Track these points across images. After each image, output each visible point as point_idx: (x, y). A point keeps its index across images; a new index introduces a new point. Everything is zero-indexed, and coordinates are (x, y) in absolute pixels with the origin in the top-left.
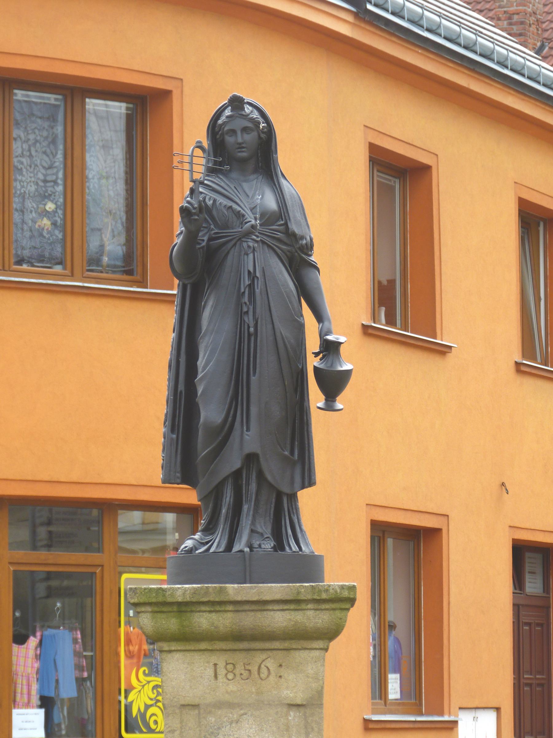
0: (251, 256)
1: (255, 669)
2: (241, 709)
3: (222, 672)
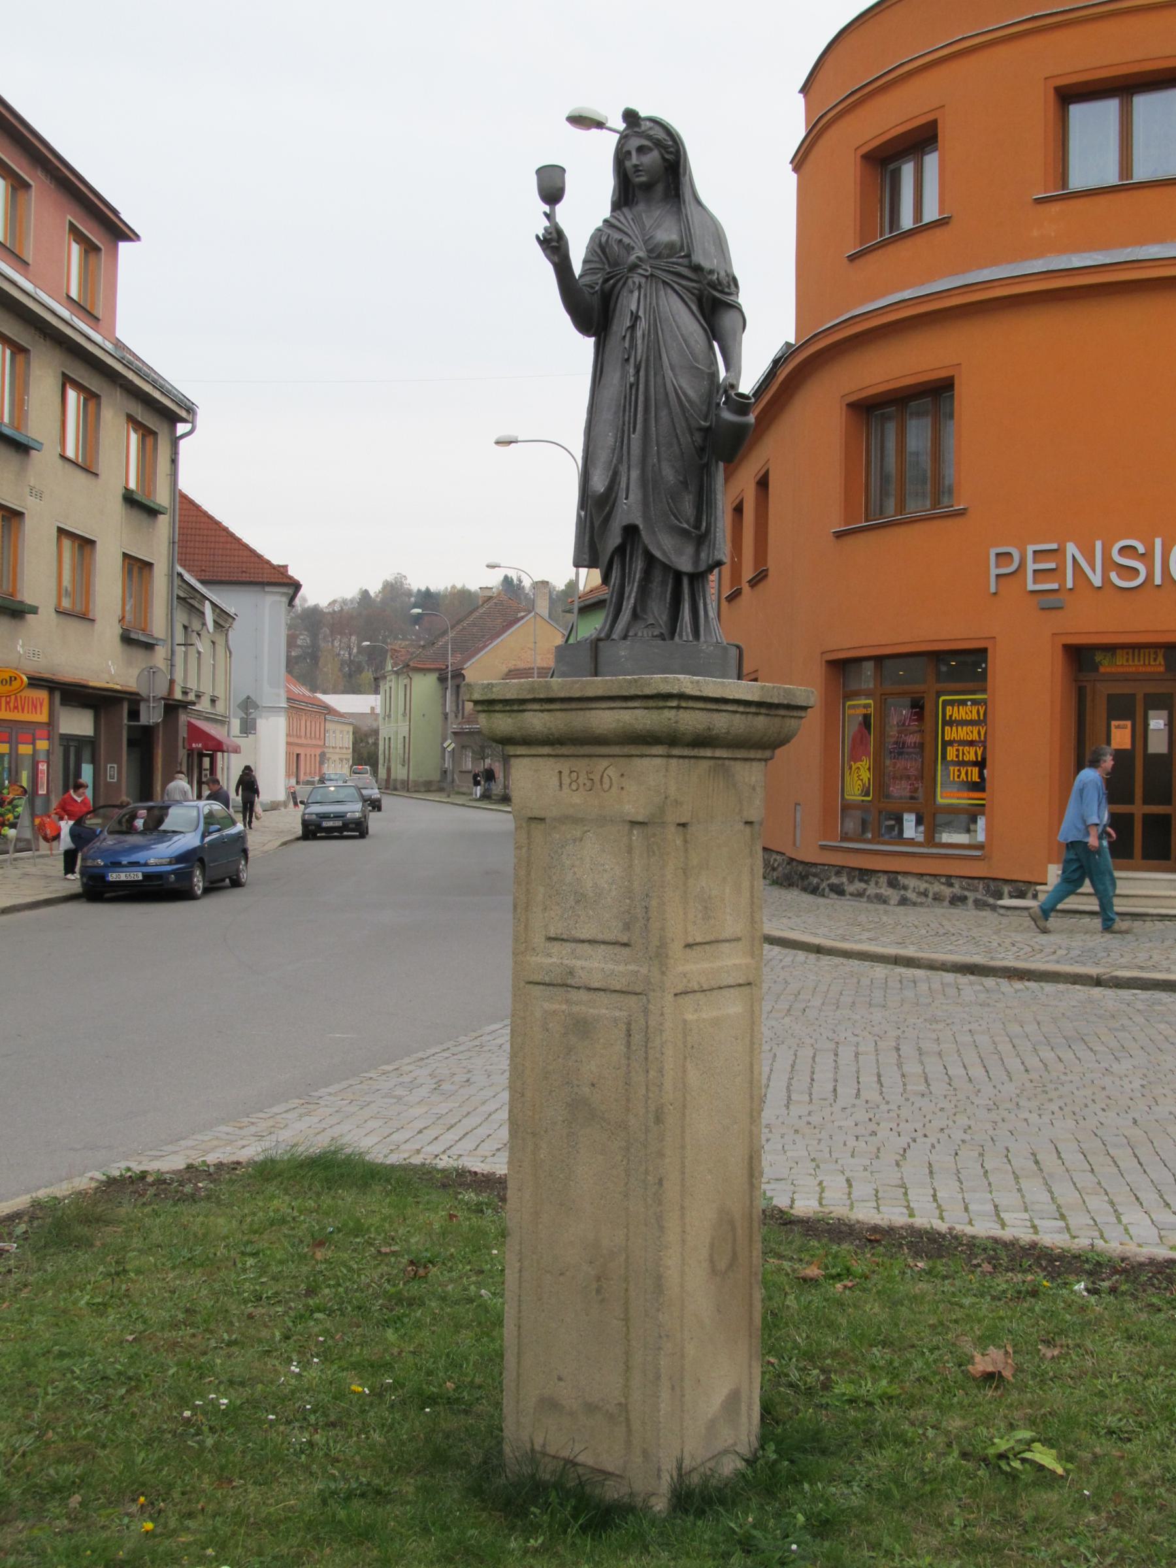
0: (636, 294)
1: (597, 778)
2: (584, 826)
3: (566, 781)
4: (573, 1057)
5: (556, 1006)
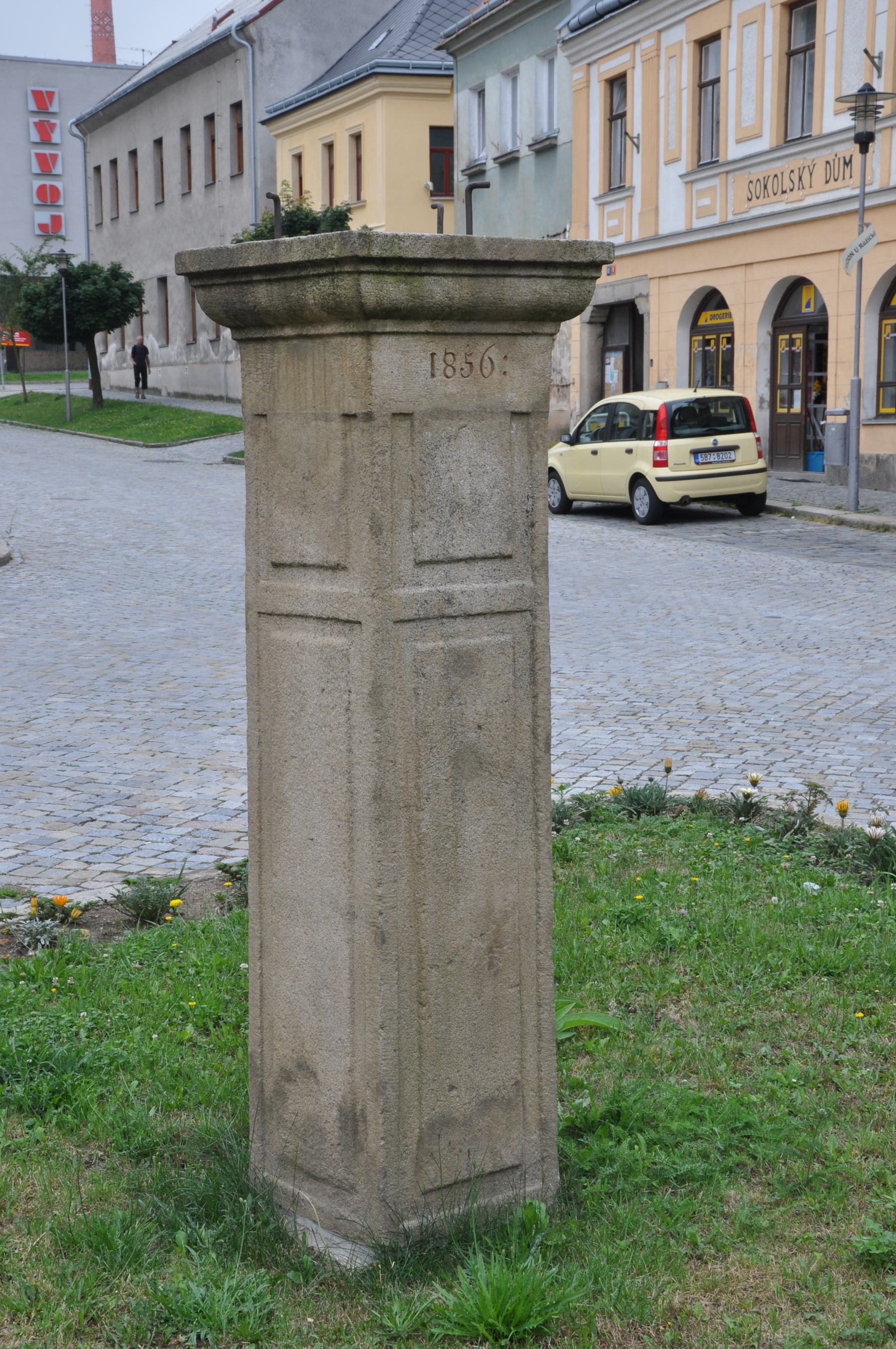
1: (476, 361)
3: (440, 365)
4: (456, 700)
5: (431, 645)
